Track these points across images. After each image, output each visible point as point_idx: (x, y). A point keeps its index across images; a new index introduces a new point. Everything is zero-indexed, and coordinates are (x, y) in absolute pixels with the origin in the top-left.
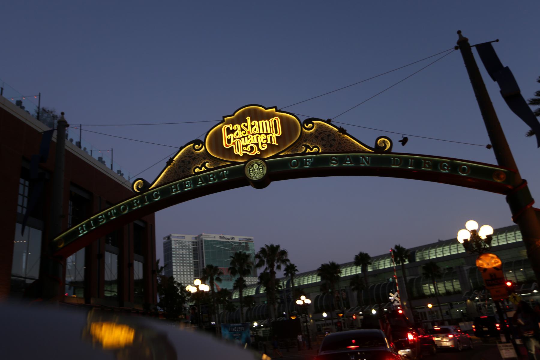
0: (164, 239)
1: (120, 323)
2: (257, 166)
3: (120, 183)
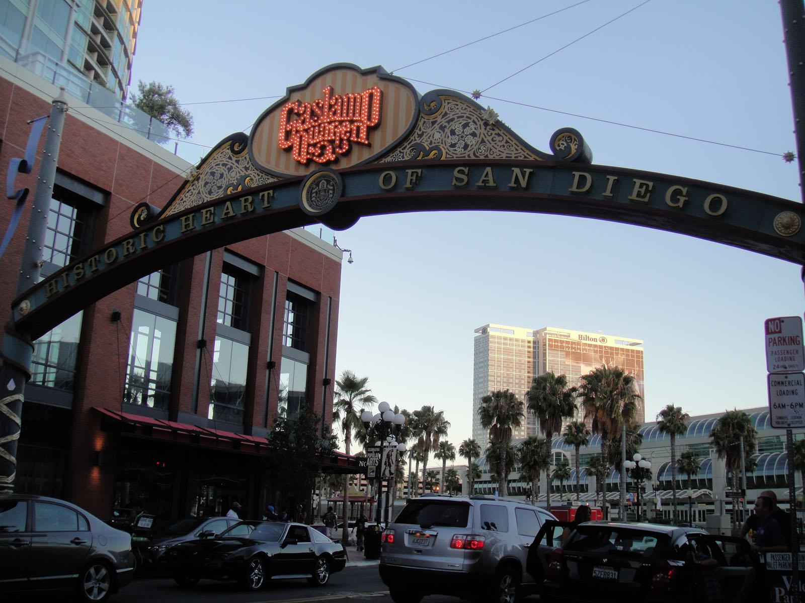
0: (476, 331)
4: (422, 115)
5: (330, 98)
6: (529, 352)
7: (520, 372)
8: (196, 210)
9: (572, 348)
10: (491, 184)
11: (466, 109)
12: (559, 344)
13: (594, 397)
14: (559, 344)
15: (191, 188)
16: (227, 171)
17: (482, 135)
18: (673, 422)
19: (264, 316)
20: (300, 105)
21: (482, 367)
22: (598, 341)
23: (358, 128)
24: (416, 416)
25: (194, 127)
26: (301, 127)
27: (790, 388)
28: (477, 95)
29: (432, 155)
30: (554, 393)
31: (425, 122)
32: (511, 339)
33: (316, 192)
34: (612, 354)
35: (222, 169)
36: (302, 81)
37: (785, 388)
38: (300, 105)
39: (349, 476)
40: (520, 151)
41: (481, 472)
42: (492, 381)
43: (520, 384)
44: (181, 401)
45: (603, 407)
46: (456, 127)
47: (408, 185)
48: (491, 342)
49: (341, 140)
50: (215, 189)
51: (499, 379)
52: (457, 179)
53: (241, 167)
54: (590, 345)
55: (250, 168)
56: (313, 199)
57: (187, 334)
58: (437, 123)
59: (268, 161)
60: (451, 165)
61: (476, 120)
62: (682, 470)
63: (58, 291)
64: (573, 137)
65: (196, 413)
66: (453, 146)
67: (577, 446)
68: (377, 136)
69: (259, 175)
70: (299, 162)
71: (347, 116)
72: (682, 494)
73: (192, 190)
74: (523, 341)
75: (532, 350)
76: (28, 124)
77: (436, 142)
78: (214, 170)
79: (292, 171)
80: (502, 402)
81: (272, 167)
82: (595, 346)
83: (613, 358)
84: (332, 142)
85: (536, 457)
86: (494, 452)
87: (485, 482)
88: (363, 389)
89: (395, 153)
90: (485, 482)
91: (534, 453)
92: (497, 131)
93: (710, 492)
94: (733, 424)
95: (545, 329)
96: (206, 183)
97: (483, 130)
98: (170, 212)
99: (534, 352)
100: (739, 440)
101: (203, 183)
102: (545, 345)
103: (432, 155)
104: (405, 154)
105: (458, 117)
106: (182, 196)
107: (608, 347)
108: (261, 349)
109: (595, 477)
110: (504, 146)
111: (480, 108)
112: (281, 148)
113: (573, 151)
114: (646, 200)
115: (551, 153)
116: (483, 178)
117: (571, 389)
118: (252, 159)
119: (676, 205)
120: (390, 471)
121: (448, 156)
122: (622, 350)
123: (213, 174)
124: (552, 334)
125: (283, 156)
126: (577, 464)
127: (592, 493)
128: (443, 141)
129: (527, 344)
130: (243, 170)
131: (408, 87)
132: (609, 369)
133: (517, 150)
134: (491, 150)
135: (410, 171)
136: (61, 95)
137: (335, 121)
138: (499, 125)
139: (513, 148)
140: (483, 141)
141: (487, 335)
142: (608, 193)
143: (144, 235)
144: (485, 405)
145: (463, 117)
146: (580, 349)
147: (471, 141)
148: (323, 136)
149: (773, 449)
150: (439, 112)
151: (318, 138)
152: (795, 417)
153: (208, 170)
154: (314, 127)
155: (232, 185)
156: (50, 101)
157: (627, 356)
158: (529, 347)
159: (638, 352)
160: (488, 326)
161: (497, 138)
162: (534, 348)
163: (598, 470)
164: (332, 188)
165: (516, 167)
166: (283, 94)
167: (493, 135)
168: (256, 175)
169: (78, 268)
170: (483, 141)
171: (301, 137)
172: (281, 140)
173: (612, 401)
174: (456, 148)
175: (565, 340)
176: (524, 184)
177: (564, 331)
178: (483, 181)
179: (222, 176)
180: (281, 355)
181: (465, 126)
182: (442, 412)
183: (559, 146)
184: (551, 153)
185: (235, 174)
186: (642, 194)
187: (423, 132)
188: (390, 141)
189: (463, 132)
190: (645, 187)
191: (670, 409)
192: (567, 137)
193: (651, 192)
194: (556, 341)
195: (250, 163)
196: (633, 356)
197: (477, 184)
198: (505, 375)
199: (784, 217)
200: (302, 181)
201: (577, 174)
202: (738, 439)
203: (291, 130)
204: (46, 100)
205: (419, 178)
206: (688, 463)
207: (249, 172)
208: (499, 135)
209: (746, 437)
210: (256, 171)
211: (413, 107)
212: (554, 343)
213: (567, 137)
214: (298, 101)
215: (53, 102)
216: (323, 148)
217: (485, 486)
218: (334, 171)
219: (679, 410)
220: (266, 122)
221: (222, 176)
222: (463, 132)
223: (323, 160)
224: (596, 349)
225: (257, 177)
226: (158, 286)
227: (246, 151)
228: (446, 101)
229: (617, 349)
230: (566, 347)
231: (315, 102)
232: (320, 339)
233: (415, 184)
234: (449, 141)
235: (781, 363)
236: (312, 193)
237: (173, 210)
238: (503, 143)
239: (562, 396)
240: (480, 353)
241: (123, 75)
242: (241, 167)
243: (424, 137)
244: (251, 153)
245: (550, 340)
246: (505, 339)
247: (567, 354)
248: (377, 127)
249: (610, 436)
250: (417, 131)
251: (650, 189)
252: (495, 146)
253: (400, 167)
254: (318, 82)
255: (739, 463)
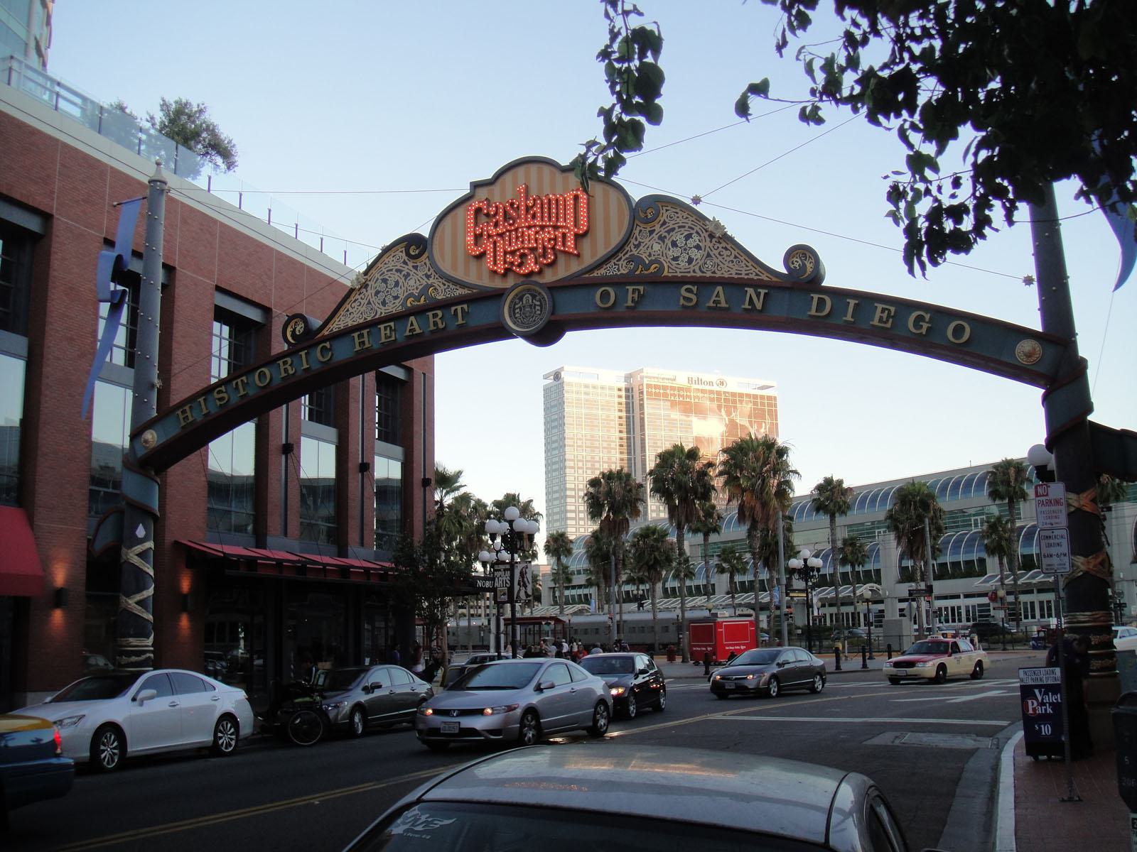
0: (546, 377)
1: (190, 589)
2: (530, 298)
3: (335, 277)
4: (637, 222)
5: (527, 198)
6: (620, 404)
7: (608, 431)
8: (372, 325)
10: (724, 304)
11: (687, 218)
12: (661, 391)
13: (739, 475)
14: (661, 391)
15: (357, 297)
16: (403, 278)
17: (707, 249)
18: (831, 497)
19: (352, 406)
20: (489, 205)
21: (556, 427)
22: (714, 384)
23: (564, 235)
24: (497, 507)
25: (239, 159)
26: (493, 231)
27: (1056, 541)
28: (697, 200)
29: (652, 269)
30: (685, 470)
31: (641, 231)
33: (520, 308)
34: (734, 402)
35: (396, 276)
36: (489, 175)
37: (1051, 541)
38: (489, 205)
40: (751, 267)
41: (573, 573)
43: (609, 449)
44: (269, 524)
45: (752, 489)
46: (678, 238)
47: (630, 303)
49: (544, 248)
50: (389, 299)
51: (580, 443)
52: (685, 298)
53: (420, 274)
54: (703, 391)
55: (432, 276)
56: (517, 315)
57: (270, 439)
58: (656, 232)
59: (454, 266)
60: (677, 282)
61: (699, 231)
62: (844, 561)
63: (195, 420)
64: (808, 254)
65: (286, 535)
66: (675, 259)
67: (706, 535)
68: (586, 244)
69: (445, 285)
70: (495, 272)
71: (550, 220)
72: (845, 591)
73: (360, 300)
74: (611, 388)
75: (623, 400)
76: (115, 206)
77: (656, 253)
78: (387, 277)
79: (487, 282)
80: (615, 485)
81: (459, 275)
82: (711, 392)
84: (533, 250)
85: (656, 553)
86: (600, 549)
87: (580, 587)
88: (458, 484)
89: (608, 265)
90: (580, 587)
91: (653, 549)
92: (724, 245)
93: (879, 587)
94: (915, 502)
95: (641, 371)
96: (377, 293)
97: (708, 243)
98: (335, 326)
99: (627, 404)
100: (923, 522)
101: (373, 292)
102: (642, 393)
103: (652, 269)
104: (620, 268)
105: (679, 227)
106: (347, 306)
107: (728, 393)
108: (351, 448)
110: (733, 262)
111: (702, 218)
112: (470, 254)
113: (809, 270)
114: (889, 325)
115: (785, 271)
116: (714, 298)
117: (704, 465)
118: (434, 264)
119: (918, 332)
120: (526, 592)
121: (670, 271)
122: (749, 396)
123: (385, 281)
124: (650, 377)
125: (473, 265)
126: (705, 556)
127: (720, 597)
128: (670, 255)
129: (617, 393)
130: (424, 277)
131: (617, 188)
132: (756, 438)
133: (747, 266)
134: (718, 265)
135: (630, 288)
136: (158, 171)
137: (535, 226)
138: (730, 240)
139: (742, 264)
140: (709, 255)
142: (849, 318)
143: (306, 354)
144: (591, 490)
145: (684, 227)
147: (695, 254)
148: (522, 242)
149: (957, 527)
150: (658, 220)
151: (516, 244)
152: (1060, 564)
153: (377, 276)
154: (510, 231)
155: (411, 295)
156: (145, 180)
157: (755, 403)
158: (620, 397)
159: (769, 398)
161: (725, 253)
162: (627, 397)
163: (732, 566)
164: (538, 303)
165: (750, 286)
166: (466, 190)
167: (720, 249)
168: (442, 286)
169: (219, 392)
170: (709, 255)
171: (495, 243)
172: (470, 245)
173: (763, 481)
174: (679, 262)
175: (670, 385)
176: (759, 305)
177: (668, 373)
178: (714, 301)
179: (397, 284)
180: (373, 454)
181: (688, 237)
182: (531, 501)
183: (793, 263)
184: (785, 271)
185: (412, 284)
186: (884, 320)
187: (640, 242)
188: (602, 252)
189: (686, 244)
190: (887, 312)
191: (828, 482)
192: (801, 255)
193: (892, 317)
194: (656, 387)
195: (432, 270)
196: (762, 404)
197: (707, 305)
199: (1026, 346)
200: (502, 294)
201: (816, 297)
202: (922, 522)
203: (481, 235)
204: (345, 283)
205: (641, 297)
206: (851, 552)
207: (431, 281)
208: (726, 249)
209: (932, 519)
210: (440, 280)
211: (627, 213)
213: (801, 255)
214: (487, 199)
215: (149, 182)
216: (523, 256)
217: (580, 592)
218: (541, 285)
219: (840, 482)
220: (448, 222)
221: (397, 284)
222: (686, 244)
223: (524, 270)
224: (712, 396)
225: (443, 287)
226: (124, 345)
227: (426, 255)
228: (664, 208)
229: (741, 395)
230: (671, 395)
231: (508, 202)
232: (415, 428)
233: (637, 303)
234: (670, 253)
235: (1048, 521)
236: (514, 310)
237: (336, 323)
238: (732, 258)
239: (695, 475)
240: (552, 407)
241: (41, 35)
242: (420, 274)
243: (641, 247)
244: (431, 258)
245: (649, 386)
246: (586, 386)
247: (673, 404)
248: (585, 234)
249: (760, 526)
250: (633, 241)
251: (892, 314)
252: (723, 261)
253: (619, 283)
254: (508, 177)
255: (923, 552)
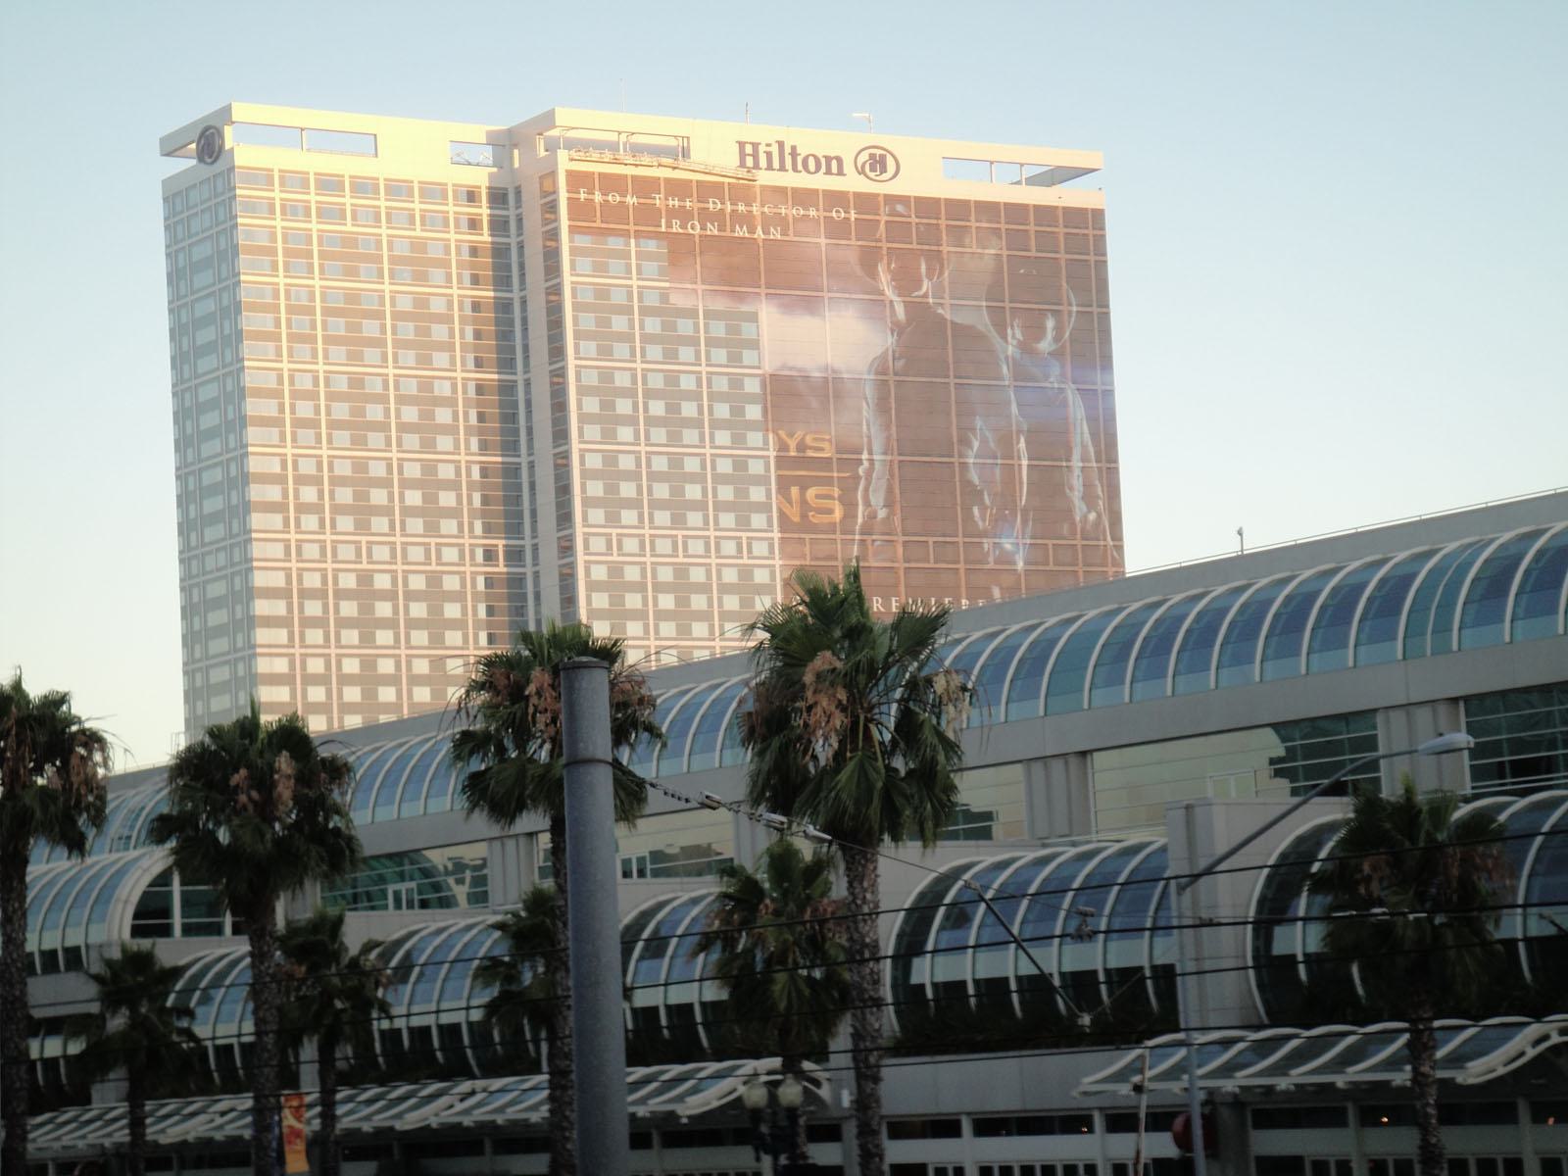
9: (705, 216)
12: (631, 200)
14: (631, 200)
22: (848, 167)
32: (363, 186)
34: (930, 235)
39: (1481, 849)
42: (264, 422)
48: (251, 207)
51: (305, 409)
54: (804, 197)
74: (433, 191)
75: (485, 237)
82: (836, 198)
83: (936, 259)
95: (548, 119)
102: (552, 207)
107: (904, 200)
109: (32, 945)
122: (988, 209)
124: (583, 146)
141: (220, 166)
146: (747, 220)
157: (1017, 240)
160: (225, 114)
162: (499, 226)
177: (656, 127)
194: (611, 183)
198: (342, 385)
212: (598, 197)
230: (672, 213)
245: (576, 180)
246: (330, 184)
